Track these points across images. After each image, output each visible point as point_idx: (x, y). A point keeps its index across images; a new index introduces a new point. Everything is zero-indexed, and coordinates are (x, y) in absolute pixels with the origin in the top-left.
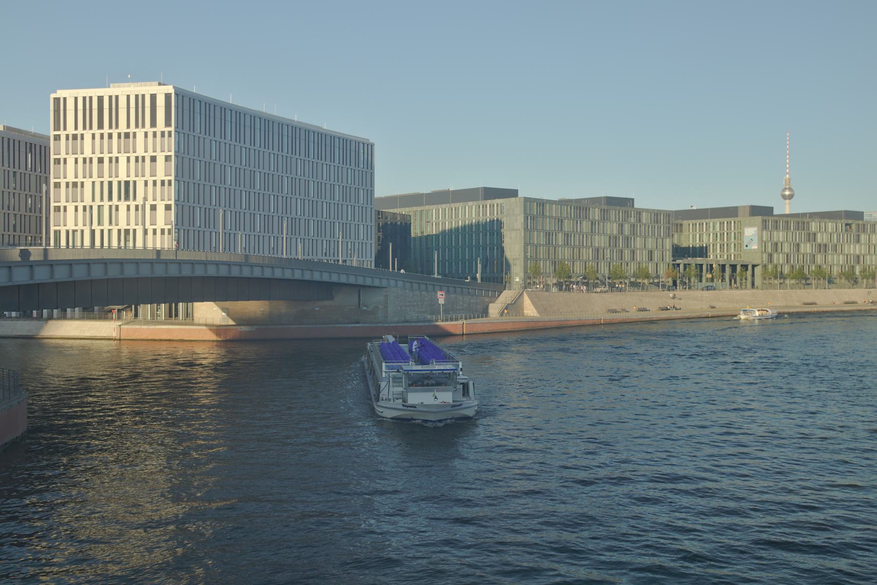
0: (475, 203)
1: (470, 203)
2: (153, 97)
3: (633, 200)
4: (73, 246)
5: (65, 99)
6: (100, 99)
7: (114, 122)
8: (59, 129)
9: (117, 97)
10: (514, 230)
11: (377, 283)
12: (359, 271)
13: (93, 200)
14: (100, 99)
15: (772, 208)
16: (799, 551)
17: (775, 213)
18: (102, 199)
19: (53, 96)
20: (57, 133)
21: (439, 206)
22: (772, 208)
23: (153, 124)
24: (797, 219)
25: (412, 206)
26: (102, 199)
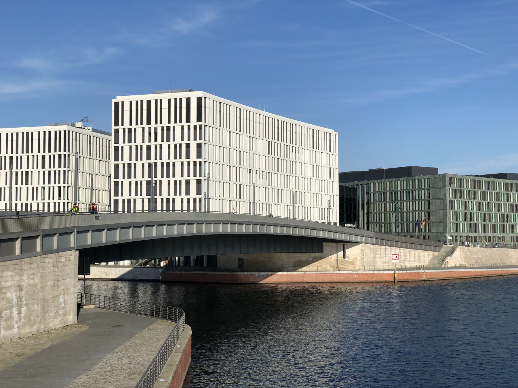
0: (405, 178)
1: (402, 179)
2: (188, 100)
3: (437, 169)
4: (174, 210)
5: (123, 103)
6: (149, 102)
7: (159, 119)
8: (118, 125)
9: (161, 100)
10: (438, 199)
12: (326, 226)
13: (182, 176)
14: (149, 102)
15: (436, 169)
16: (10, 165)
18: (44, 151)
19: (114, 101)
20: (117, 127)
22: (436, 169)
23: (188, 120)
25: (354, 181)
26: (44, 151)
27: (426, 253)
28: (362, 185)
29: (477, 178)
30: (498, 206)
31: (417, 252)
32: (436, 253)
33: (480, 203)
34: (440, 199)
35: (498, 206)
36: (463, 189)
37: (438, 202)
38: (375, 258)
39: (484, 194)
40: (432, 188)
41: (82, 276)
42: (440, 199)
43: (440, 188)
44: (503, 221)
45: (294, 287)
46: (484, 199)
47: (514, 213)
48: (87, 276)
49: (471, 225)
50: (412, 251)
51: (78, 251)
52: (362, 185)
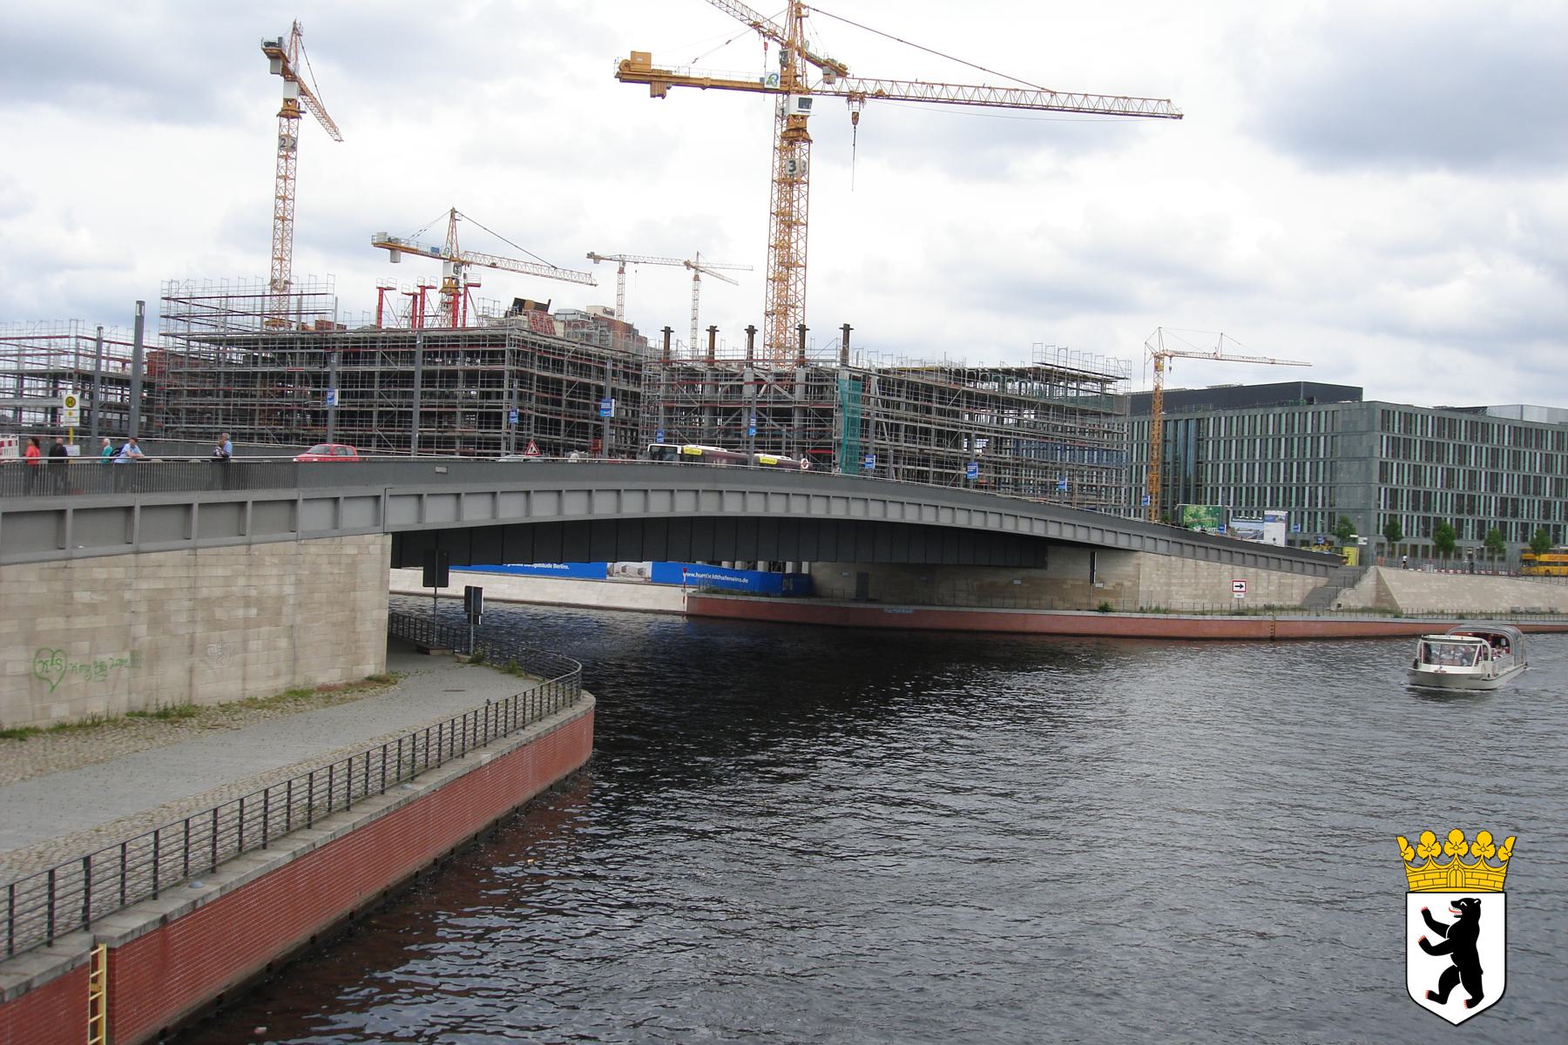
1: (1278, 410)
10: (1355, 459)
17: (1365, 399)
21: (1245, 412)
27: (1298, 579)
28: (1217, 420)
29: (1447, 415)
30: (1494, 480)
31: (1275, 576)
32: (1322, 581)
33: (1450, 472)
34: (1360, 459)
35: (1494, 480)
36: (375, 410)
37: (1355, 465)
38: (1169, 584)
39: (1462, 451)
40: (1344, 434)
41: (431, 590)
42: (1360, 459)
43: (1362, 433)
44: (1504, 514)
45: (51, 977)
46: (1462, 462)
47: (1531, 497)
48: (441, 591)
49: (1427, 509)
50: (1263, 574)
51: (390, 537)
52: (1217, 420)
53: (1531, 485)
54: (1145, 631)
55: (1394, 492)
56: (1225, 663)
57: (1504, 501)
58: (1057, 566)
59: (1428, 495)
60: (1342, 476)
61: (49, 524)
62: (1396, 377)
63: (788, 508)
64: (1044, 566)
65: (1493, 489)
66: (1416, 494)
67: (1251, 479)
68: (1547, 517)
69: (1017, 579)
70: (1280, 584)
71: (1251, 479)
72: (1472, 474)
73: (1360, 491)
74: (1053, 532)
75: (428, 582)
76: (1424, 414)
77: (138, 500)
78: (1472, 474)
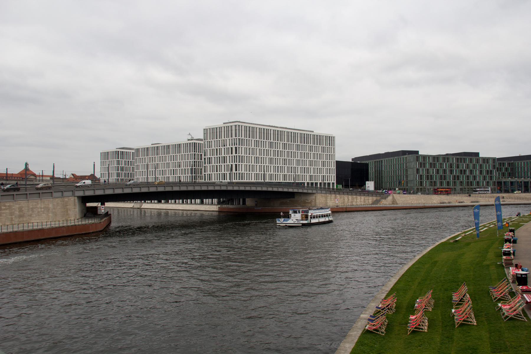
11: (310, 191)
24: (458, 157)
27: (371, 198)
30: (451, 172)
33: (438, 170)
50: (359, 197)
53: (463, 172)
54: (381, 208)
55: (421, 176)
56: (412, 215)
57: (454, 176)
58: (297, 198)
59: (431, 176)
60: (409, 173)
61: (38, 195)
62: (430, 148)
63: (132, 191)
64: (294, 198)
65: (451, 174)
66: (428, 176)
67: (398, 174)
68: (468, 179)
69: (288, 200)
70: (364, 199)
71: (398, 174)
72: (445, 170)
73: (412, 176)
74: (295, 190)
75: (101, 205)
76: (429, 156)
77: (15, 193)
78: (445, 170)
